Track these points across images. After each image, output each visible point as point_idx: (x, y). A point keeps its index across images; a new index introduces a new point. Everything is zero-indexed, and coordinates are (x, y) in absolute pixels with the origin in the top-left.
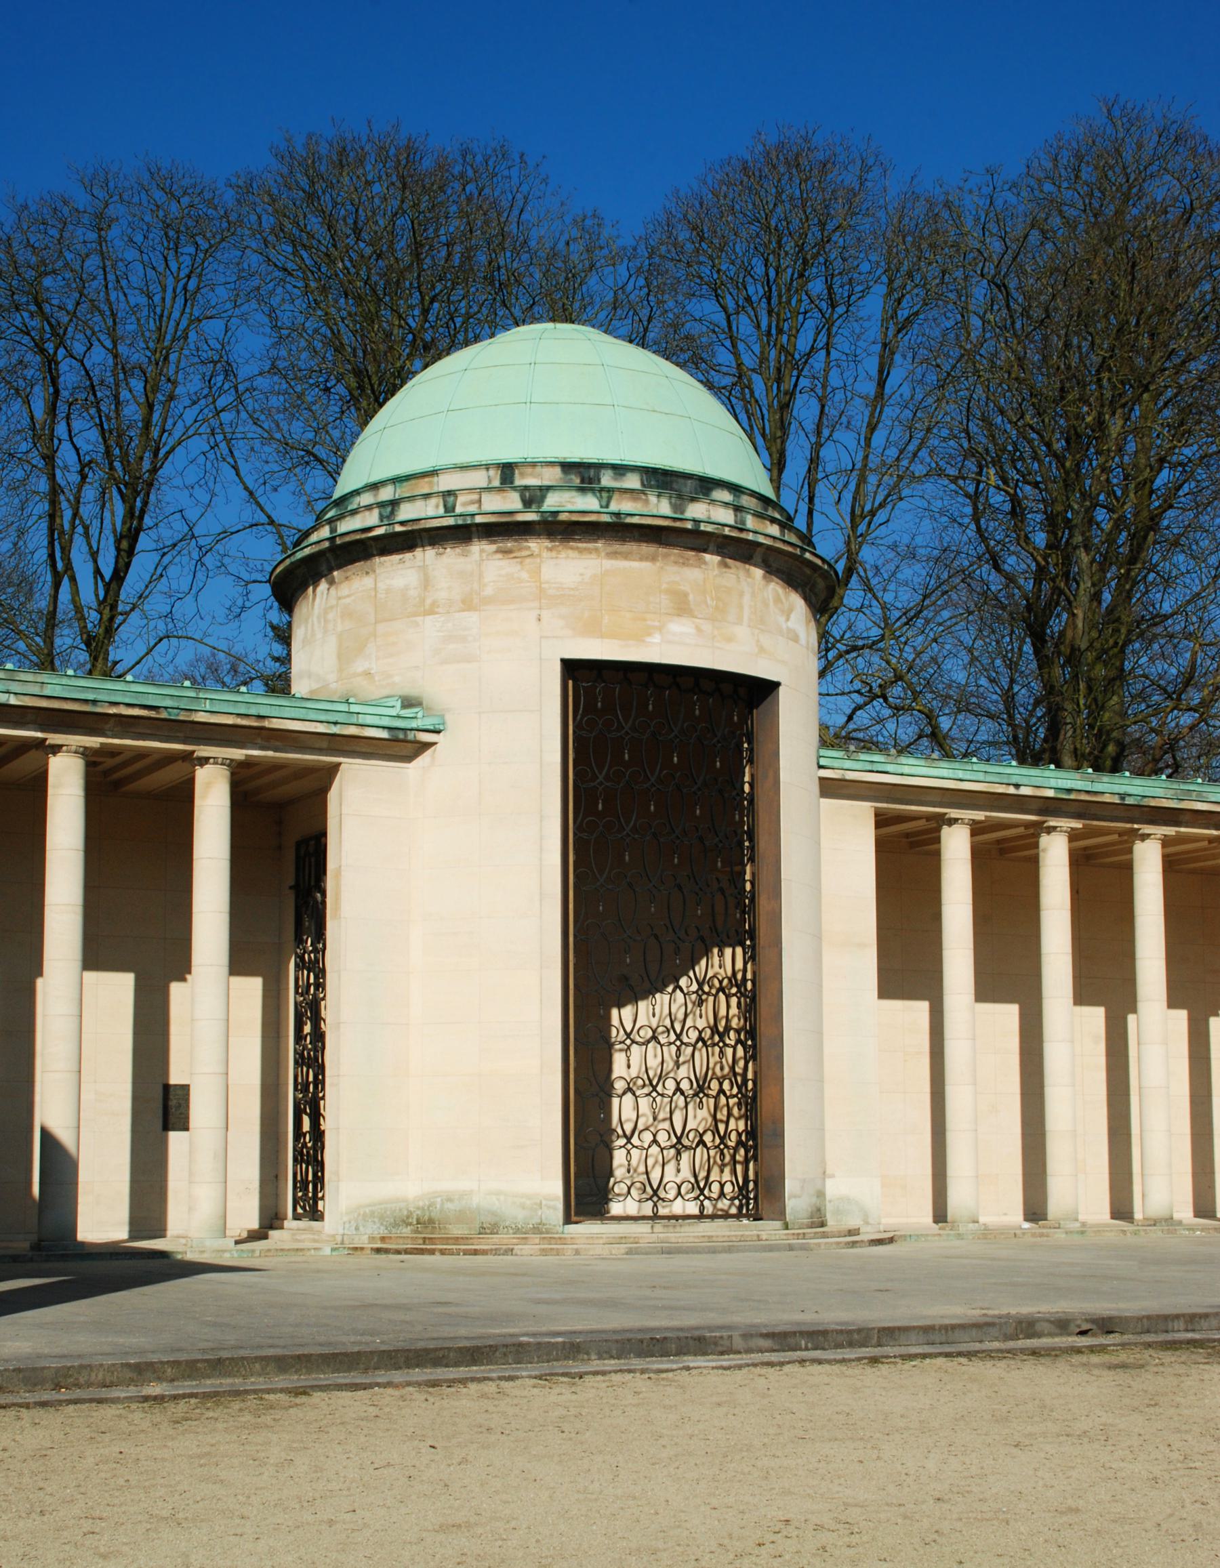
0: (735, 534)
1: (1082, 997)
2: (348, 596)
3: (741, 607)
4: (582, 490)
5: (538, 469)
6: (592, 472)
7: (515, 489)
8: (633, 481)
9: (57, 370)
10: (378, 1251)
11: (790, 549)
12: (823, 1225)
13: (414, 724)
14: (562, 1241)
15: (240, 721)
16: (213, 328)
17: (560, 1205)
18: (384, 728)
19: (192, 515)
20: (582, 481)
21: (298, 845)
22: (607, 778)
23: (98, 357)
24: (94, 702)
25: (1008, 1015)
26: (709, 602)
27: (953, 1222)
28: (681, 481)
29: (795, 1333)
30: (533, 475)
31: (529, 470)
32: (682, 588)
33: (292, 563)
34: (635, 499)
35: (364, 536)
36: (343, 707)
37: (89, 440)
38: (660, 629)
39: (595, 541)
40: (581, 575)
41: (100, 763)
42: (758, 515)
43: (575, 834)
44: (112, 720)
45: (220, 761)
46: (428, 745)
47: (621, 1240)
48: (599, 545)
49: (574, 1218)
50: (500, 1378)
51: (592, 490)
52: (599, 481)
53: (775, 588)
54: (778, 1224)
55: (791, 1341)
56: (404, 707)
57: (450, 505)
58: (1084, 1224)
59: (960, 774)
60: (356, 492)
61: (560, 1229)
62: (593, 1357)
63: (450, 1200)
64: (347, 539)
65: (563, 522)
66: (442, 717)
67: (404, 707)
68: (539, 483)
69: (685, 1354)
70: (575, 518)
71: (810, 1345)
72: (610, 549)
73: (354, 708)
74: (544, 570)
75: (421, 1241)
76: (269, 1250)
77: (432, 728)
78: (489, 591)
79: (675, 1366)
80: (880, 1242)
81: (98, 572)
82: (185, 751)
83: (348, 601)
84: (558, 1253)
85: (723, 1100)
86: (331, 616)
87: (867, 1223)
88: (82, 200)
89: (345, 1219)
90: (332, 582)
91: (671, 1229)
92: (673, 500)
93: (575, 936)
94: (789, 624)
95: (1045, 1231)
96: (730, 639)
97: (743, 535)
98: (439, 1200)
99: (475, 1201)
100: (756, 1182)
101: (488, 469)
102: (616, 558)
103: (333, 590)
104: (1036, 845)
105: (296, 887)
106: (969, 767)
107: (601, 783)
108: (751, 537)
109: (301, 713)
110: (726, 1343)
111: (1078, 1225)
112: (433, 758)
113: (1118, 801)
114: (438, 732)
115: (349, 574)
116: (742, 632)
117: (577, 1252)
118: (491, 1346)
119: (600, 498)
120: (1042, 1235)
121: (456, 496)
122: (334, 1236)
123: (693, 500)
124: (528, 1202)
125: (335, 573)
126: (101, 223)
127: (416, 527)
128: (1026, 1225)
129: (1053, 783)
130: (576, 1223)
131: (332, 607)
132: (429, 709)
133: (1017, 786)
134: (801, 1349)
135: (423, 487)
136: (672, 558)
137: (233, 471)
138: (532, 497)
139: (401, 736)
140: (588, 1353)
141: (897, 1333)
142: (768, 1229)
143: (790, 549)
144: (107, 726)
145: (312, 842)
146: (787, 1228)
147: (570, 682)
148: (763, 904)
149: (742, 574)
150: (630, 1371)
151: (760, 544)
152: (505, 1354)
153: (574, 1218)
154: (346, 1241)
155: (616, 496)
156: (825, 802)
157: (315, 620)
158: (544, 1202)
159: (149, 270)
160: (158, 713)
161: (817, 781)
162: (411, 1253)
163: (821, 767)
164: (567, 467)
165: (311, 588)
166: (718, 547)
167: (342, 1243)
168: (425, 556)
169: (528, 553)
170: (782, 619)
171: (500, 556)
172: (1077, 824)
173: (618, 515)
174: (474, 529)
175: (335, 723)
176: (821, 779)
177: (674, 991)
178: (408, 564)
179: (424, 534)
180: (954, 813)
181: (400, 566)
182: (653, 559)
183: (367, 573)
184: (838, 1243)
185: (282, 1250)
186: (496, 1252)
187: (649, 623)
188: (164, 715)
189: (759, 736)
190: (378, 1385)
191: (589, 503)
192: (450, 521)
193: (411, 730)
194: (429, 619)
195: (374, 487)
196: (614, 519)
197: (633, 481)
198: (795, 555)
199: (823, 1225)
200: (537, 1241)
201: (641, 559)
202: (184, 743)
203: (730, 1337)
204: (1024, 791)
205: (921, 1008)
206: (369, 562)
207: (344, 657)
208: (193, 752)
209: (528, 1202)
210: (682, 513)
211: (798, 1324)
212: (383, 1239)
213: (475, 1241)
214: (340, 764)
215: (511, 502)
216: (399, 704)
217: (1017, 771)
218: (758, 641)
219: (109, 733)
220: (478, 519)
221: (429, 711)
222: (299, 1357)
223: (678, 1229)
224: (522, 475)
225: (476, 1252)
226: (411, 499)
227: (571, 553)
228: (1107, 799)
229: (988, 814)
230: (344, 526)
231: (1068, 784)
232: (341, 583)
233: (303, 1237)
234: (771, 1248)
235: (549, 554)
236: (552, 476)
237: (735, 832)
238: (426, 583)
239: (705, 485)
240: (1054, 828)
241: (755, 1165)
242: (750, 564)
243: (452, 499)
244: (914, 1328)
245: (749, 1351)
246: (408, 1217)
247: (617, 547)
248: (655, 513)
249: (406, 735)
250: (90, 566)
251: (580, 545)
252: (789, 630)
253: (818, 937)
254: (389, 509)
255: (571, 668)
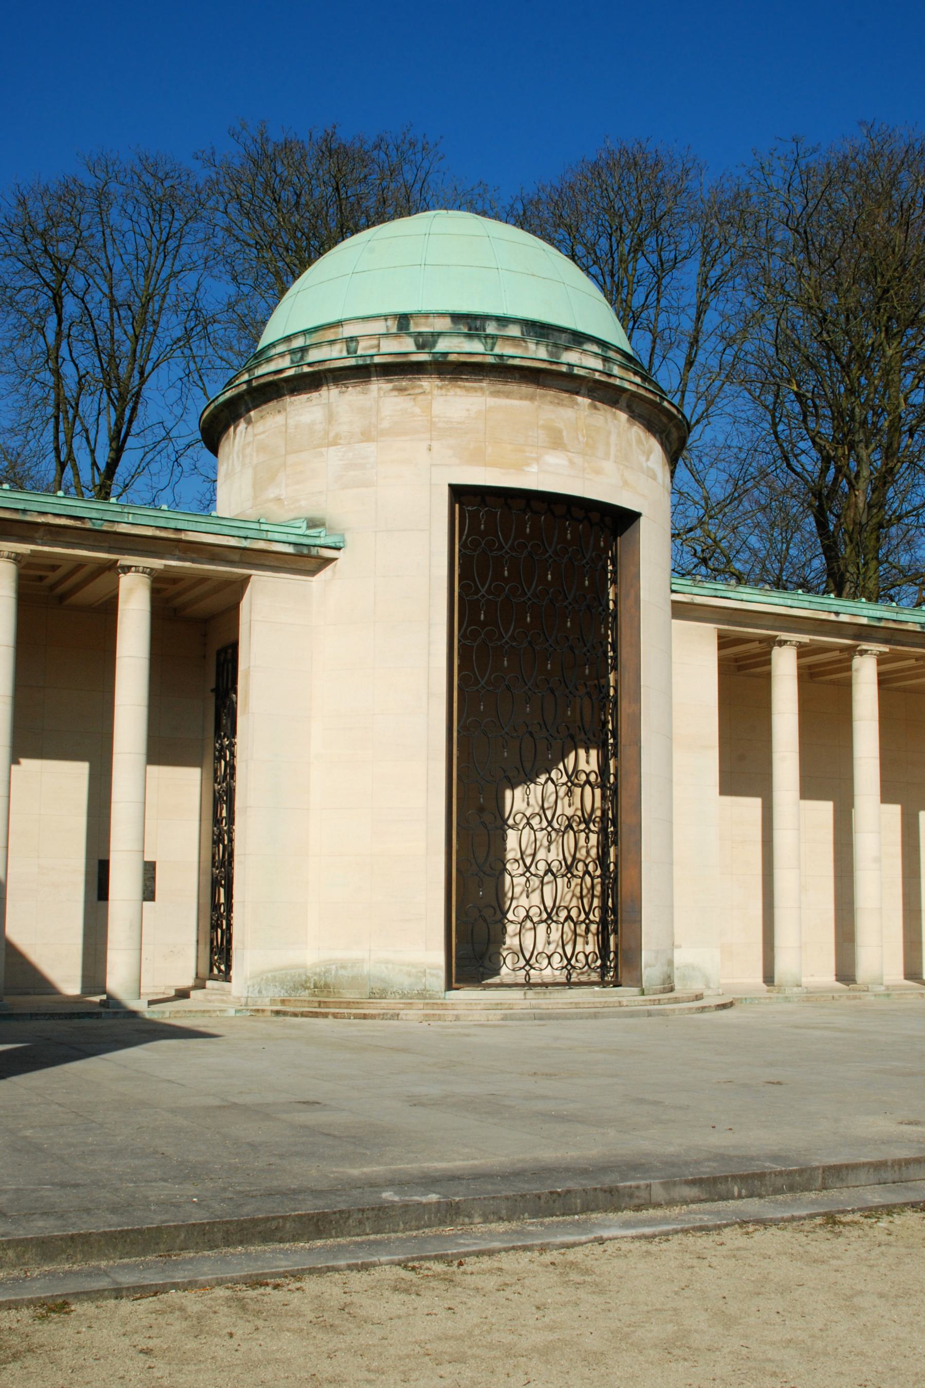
0: (604, 378)
1: (887, 796)
2: (264, 432)
3: (608, 444)
4: (469, 336)
5: (431, 320)
6: (478, 323)
7: (410, 334)
8: (514, 331)
9: (61, 303)
10: (278, 1013)
11: (651, 396)
12: (672, 990)
13: (318, 542)
14: (444, 1007)
15: (159, 533)
16: (190, 280)
17: (442, 974)
18: (290, 543)
19: (169, 425)
20: (470, 329)
21: (219, 653)
22: (489, 591)
23: (95, 298)
24: (24, 511)
25: (824, 810)
26: (581, 438)
27: (780, 986)
28: (556, 334)
29: (726, 1178)
30: (426, 325)
31: (423, 320)
32: (557, 425)
33: (216, 407)
34: (517, 346)
35: (276, 377)
36: (256, 526)
37: (88, 362)
38: (537, 460)
39: (481, 381)
40: (468, 410)
41: (46, 577)
42: (622, 366)
43: (459, 641)
44: (42, 529)
45: (141, 569)
46: (329, 561)
47: (497, 1006)
48: (484, 384)
49: (455, 985)
50: (350, 1267)
51: (478, 336)
52: (484, 330)
53: (637, 432)
54: (635, 990)
55: (721, 1187)
56: (309, 527)
57: (352, 349)
58: (888, 988)
59: (789, 602)
60: (273, 345)
61: (442, 995)
62: (477, 1220)
63: (343, 967)
64: (262, 381)
65: (452, 363)
66: (343, 536)
67: (309, 527)
68: (432, 330)
69: (593, 1210)
70: (463, 359)
71: (744, 1192)
72: (493, 388)
73: (264, 527)
74: (435, 405)
75: (316, 1005)
76: (178, 1012)
77: (333, 545)
78: (385, 424)
79: (583, 1238)
80: (723, 1006)
81: (94, 463)
82: (111, 560)
83: (263, 436)
84: (440, 1018)
85: (588, 879)
86: (248, 451)
87: (709, 988)
88: (88, 180)
89: (249, 983)
90: (249, 422)
91: (542, 996)
92: (550, 348)
93: (458, 732)
94: (649, 464)
95: (857, 994)
96: (598, 472)
97: (611, 380)
98: (334, 967)
99: (366, 968)
100: (616, 953)
101: (386, 320)
102: (499, 397)
103: (250, 429)
104: (849, 669)
105: (216, 690)
106: (796, 597)
107: (483, 596)
108: (618, 382)
109: (216, 529)
110: (643, 1194)
111: (883, 988)
112: (334, 572)
113: (919, 630)
114: (339, 549)
115: (264, 413)
116: (609, 466)
117: (457, 1018)
118: (341, 1212)
119: (485, 345)
120: (855, 998)
121: (358, 342)
122: (239, 998)
123: (567, 349)
124: (414, 971)
125: (252, 413)
126: (102, 196)
127: (322, 367)
128: (839, 985)
129: (865, 612)
130: (457, 989)
131: (249, 444)
132: (331, 528)
133: (837, 614)
134: (733, 1198)
135: (330, 335)
136: (549, 398)
137: (202, 392)
138: (425, 341)
139: (305, 551)
140: (470, 1216)
141: (844, 1172)
142: (626, 995)
143: (651, 396)
144: (37, 535)
145: (230, 651)
146: (643, 994)
147: (457, 506)
148: (625, 706)
149: (609, 416)
150: (525, 1248)
151: (625, 390)
152: (361, 1222)
153: (455, 985)
154: (250, 1003)
155: (499, 342)
156: (676, 623)
157: (235, 456)
158: (428, 971)
159: (138, 237)
160: (83, 523)
161: (670, 603)
162: (306, 1016)
163: (673, 591)
164: (457, 318)
165: (232, 428)
166: (589, 391)
167: (246, 1005)
168: (330, 394)
169: (420, 391)
170: (643, 459)
171: (396, 393)
172: (885, 648)
173: (501, 356)
174: (373, 369)
175: (246, 538)
176: (674, 602)
177: (546, 782)
178: (314, 402)
179: (329, 374)
180: (783, 636)
181: (308, 404)
182: (532, 398)
183: (279, 412)
184: (690, 1009)
185: (190, 1011)
186: (383, 1017)
187: (527, 454)
188: (89, 525)
189: (623, 560)
190: (175, 1286)
191: (477, 346)
192: (352, 362)
193: (315, 546)
194: (332, 449)
195: (288, 339)
196: (497, 361)
197: (514, 331)
198: (655, 402)
199: (672, 990)
200: (421, 1006)
201: (521, 398)
202: (109, 552)
203: (649, 1186)
204: (843, 618)
205: (754, 804)
206: (281, 403)
207: (258, 486)
208: (117, 561)
209: (414, 971)
210: (559, 358)
211: (722, 1158)
212: (283, 1002)
213: (365, 1006)
214: (250, 576)
215: (407, 345)
216: (304, 525)
217: (835, 602)
218: (622, 475)
219: (40, 541)
220: (377, 360)
221: (331, 531)
222: (72, 1238)
223: (548, 996)
224: (416, 325)
225: (365, 1017)
226: (318, 345)
227: (458, 391)
228: (910, 627)
229: (812, 637)
230: (259, 372)
231: (878, 614)
232: (257, 422)
233: (214, 997)
234: (632, 1014)
235: (439, 392)
236: (444, 324)
237: (601, 643)
238: (330, 418)
239: (578, 339)
240: (866, 651)
241: (615, 938)
242: (616, 408)
243: (353, 344)
244: (864, 1165)
245: (671, 1203)
246: (306, 982)
247: (500, 387)
248: (534, 356)
249: (309, 551)
250: (89, 461)
251: (467, 384)
252: (648, 468)
253: (669, 738)
254: (299, 355)
255: (458, 493)
